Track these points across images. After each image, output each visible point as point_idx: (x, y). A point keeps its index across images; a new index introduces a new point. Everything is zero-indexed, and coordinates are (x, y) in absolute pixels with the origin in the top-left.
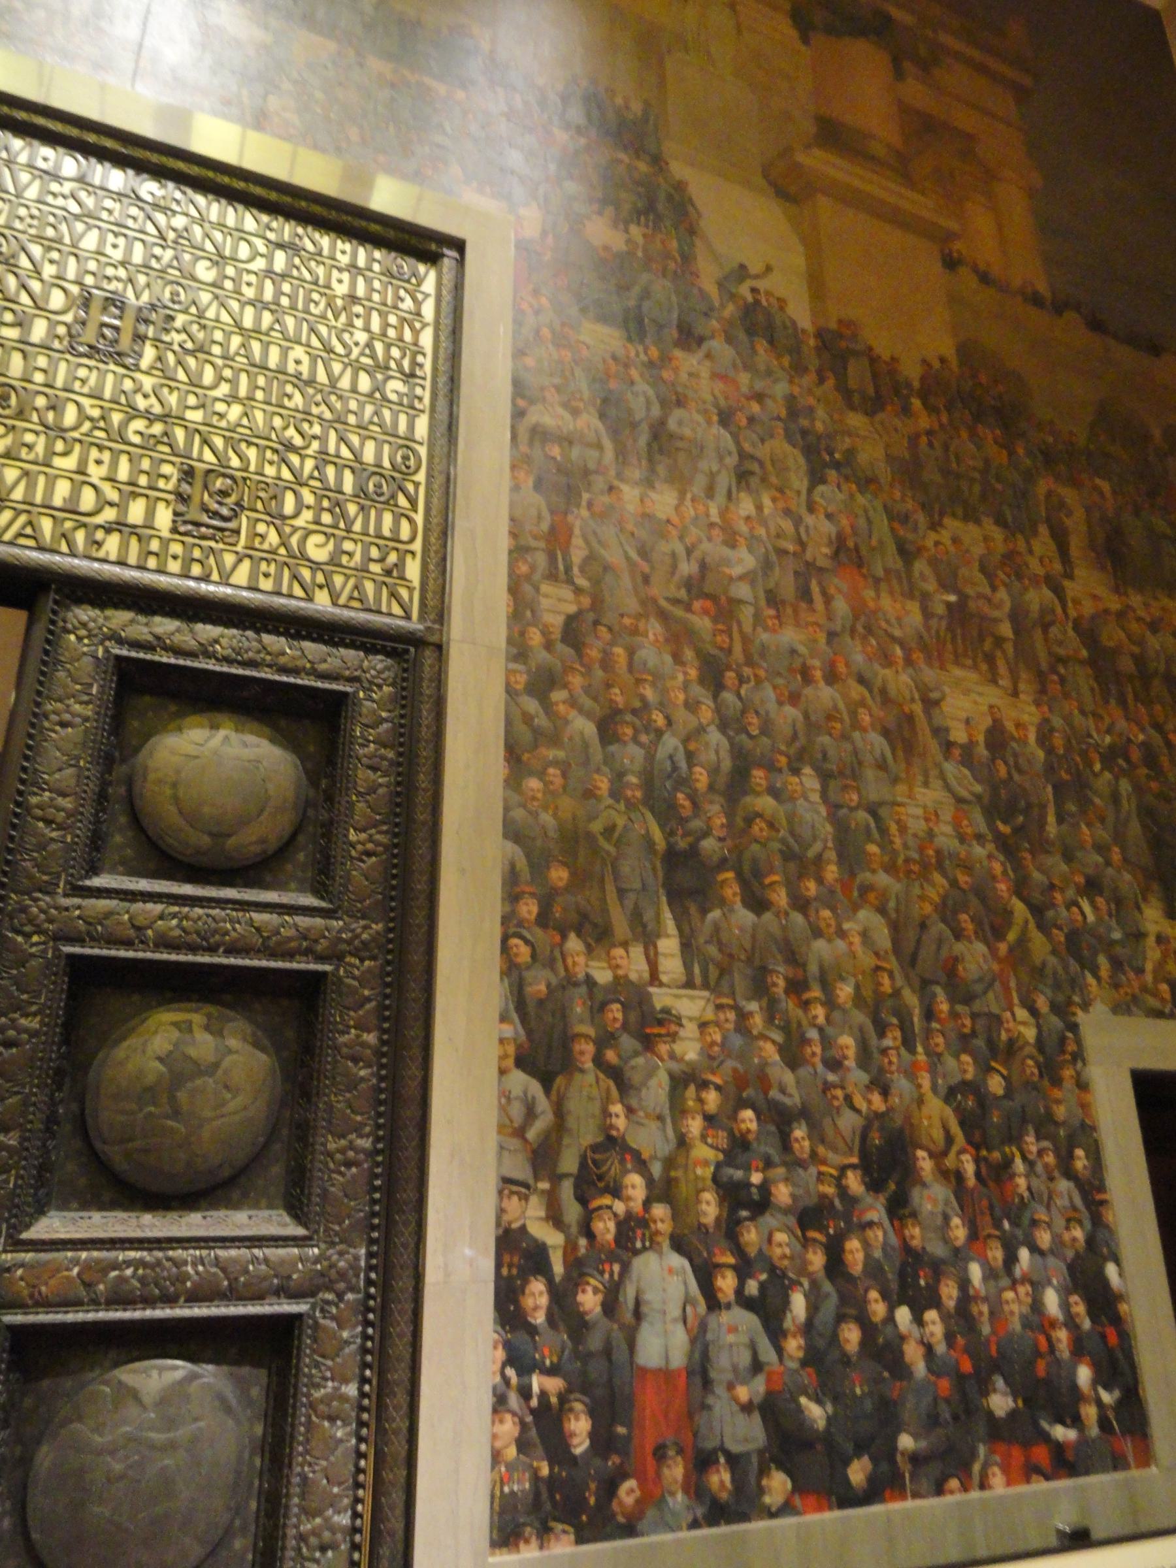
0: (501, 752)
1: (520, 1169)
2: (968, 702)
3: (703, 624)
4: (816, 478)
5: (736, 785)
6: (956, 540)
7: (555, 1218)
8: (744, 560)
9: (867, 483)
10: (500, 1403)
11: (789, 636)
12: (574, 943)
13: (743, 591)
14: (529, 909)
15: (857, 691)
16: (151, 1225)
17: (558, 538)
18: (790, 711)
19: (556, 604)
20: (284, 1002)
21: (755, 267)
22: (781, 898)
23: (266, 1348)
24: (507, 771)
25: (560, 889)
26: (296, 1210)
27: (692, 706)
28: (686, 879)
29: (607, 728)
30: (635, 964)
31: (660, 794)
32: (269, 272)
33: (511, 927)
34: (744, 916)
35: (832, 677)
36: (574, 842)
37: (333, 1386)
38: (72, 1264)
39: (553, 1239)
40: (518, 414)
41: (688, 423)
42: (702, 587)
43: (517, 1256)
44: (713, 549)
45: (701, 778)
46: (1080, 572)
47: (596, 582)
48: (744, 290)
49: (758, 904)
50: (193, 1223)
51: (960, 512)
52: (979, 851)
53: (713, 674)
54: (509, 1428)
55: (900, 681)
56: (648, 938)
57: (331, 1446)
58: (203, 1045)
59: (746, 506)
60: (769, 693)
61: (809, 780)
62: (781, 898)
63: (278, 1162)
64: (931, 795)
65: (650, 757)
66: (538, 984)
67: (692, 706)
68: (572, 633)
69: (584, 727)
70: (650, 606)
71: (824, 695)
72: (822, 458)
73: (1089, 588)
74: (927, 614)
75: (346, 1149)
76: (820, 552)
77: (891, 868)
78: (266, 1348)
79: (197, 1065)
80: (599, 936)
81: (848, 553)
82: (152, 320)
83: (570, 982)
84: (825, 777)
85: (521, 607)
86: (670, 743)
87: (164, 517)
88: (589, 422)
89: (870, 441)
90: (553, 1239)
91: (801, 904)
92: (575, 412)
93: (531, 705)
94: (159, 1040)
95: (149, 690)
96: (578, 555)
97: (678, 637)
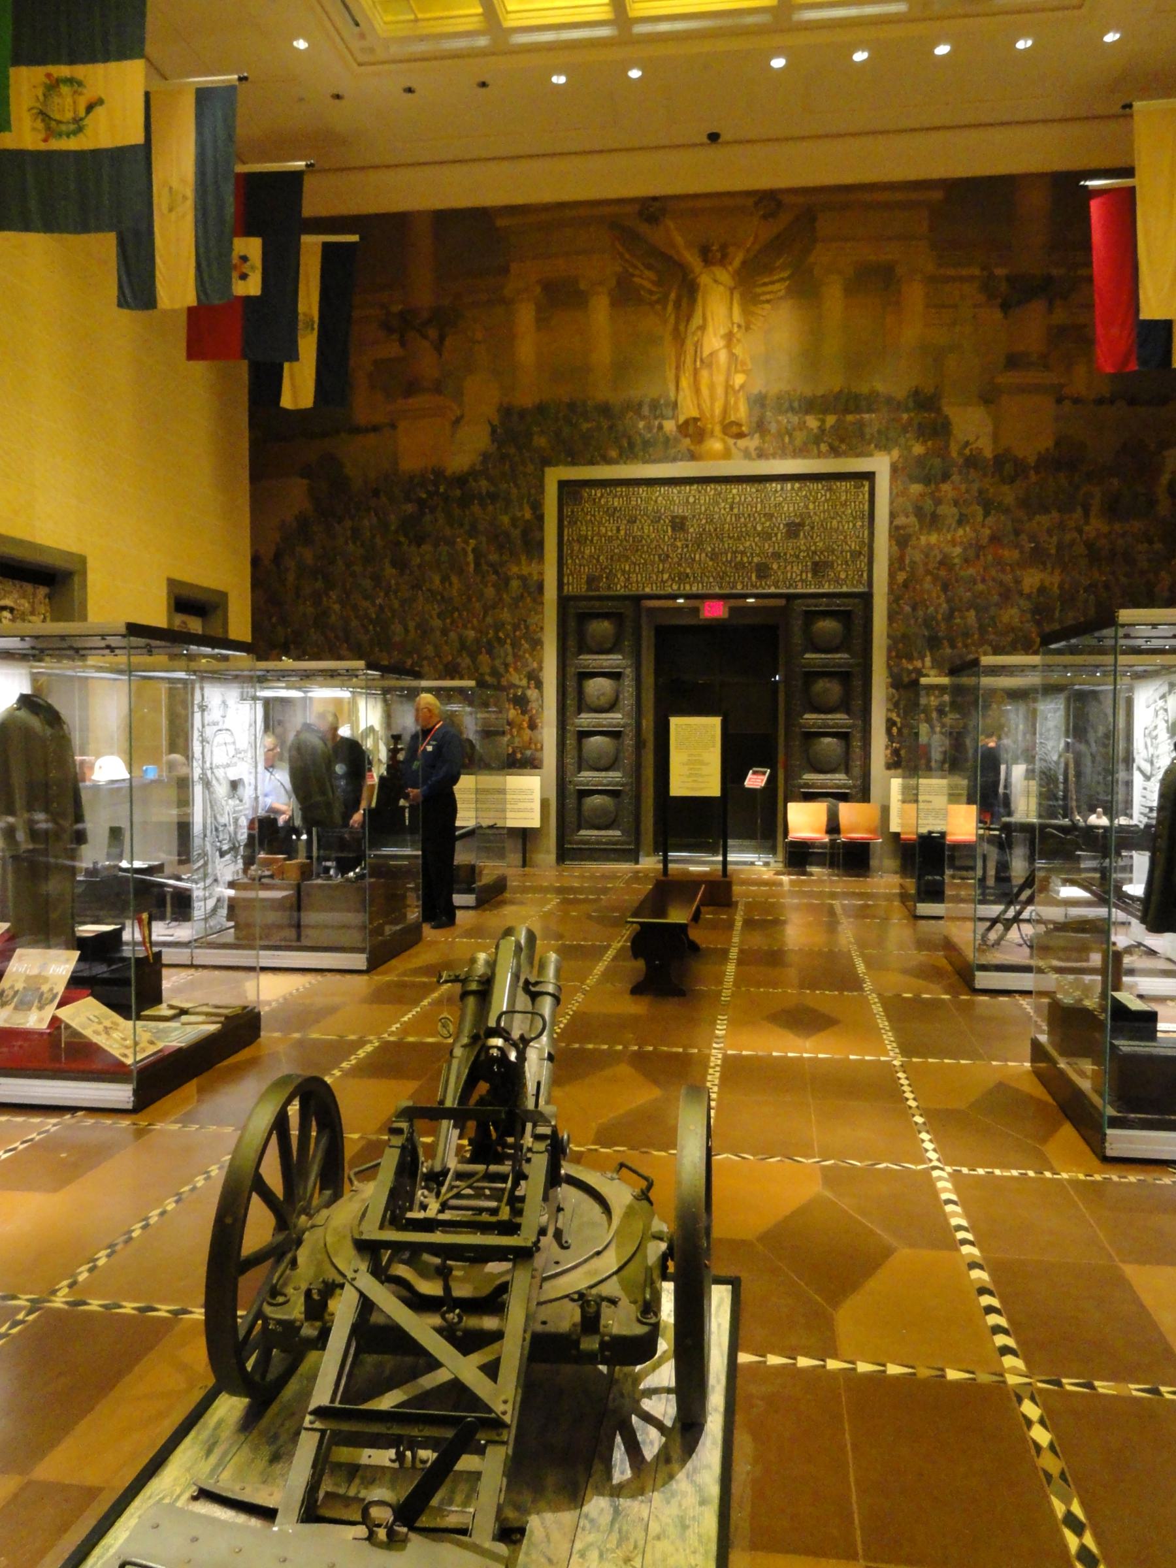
0: (406, 1309)
1: (891, 707)
2: (1031, 579)
3: (943, 573)
4: (987, 514)
5: (950, 617)
6: (1039, 523)
7: (898, 716)
8: (958, 550)
9: (1007, 511)
10: (887, 747)
11: (971, 571)
12: (904, 661)
13: (956, 561)
14: (894, 654)
15: (991, 583)
16: (822, 716)
17: (901, 559)
18: (968, 594)
19: (901, 577)
20: (844, 677)
21: (972, 439)
22: (960, 645)
23: (844, 737)
24: (642, 978)
25: (900, 648)
26: (848, 714)
27: (938, 597)
28: (933, 643)
29: (914, 608)
30: (919, 664)
31: (927, 622)
32: (826, 500)
33: (889, 658)
34: (948, 651)
35: (983, 581)
36: (905, 637)
37: (856, 743)
38: (811, 722)
39: (898, 720)
40: (891, 523)
41: (943, 510)
42: (945, 562)
43: (890, 723)
44: (947, 549)
45: (940, 617)
46: (1093, 521)
47: (912, 568)
48: (967, 451)
49: (953, 646)
50: (829, 716)
51: (989, 649)
52: (1027, 625)
53: (945, 587)
54: (889, 751)
55: (1008, 578)
56: (922, 658)
57: (857, 751)
58: (828, 685)
59: (961, 532)
60: (962, 589)
61: (972, 613)
62: (960, 645)
63: (844, 706)
64: (1014, 611)
65: (925, 614)
66: (895, 670)
67: (938, 597)
68: (906, 585)
69: (908, 609)
70: (928, 572)
71: (980, 587)
72: (988, 506)
73: (1096, 525)
74: (1022, 552)
75: (857, 703)
76: (984, 542)
77: (995, 633)
78: (844, 737)
79: (830, 689)
80: (910, 658)
81: (995, 539)
82: (801, 525)
83: (902, 669)
84: (977, 612)
85: (892, 575)
86: (931, 609)
87: (810, 575)
88: (913, 519)
89: (1008, 495)
90: (898, 720)
91: (966, 646)
92: (907, 517)
93: (894, 606)
94: (821, 685)
95: (811, 616)
96: (907, 562)
97: (936, 578)
